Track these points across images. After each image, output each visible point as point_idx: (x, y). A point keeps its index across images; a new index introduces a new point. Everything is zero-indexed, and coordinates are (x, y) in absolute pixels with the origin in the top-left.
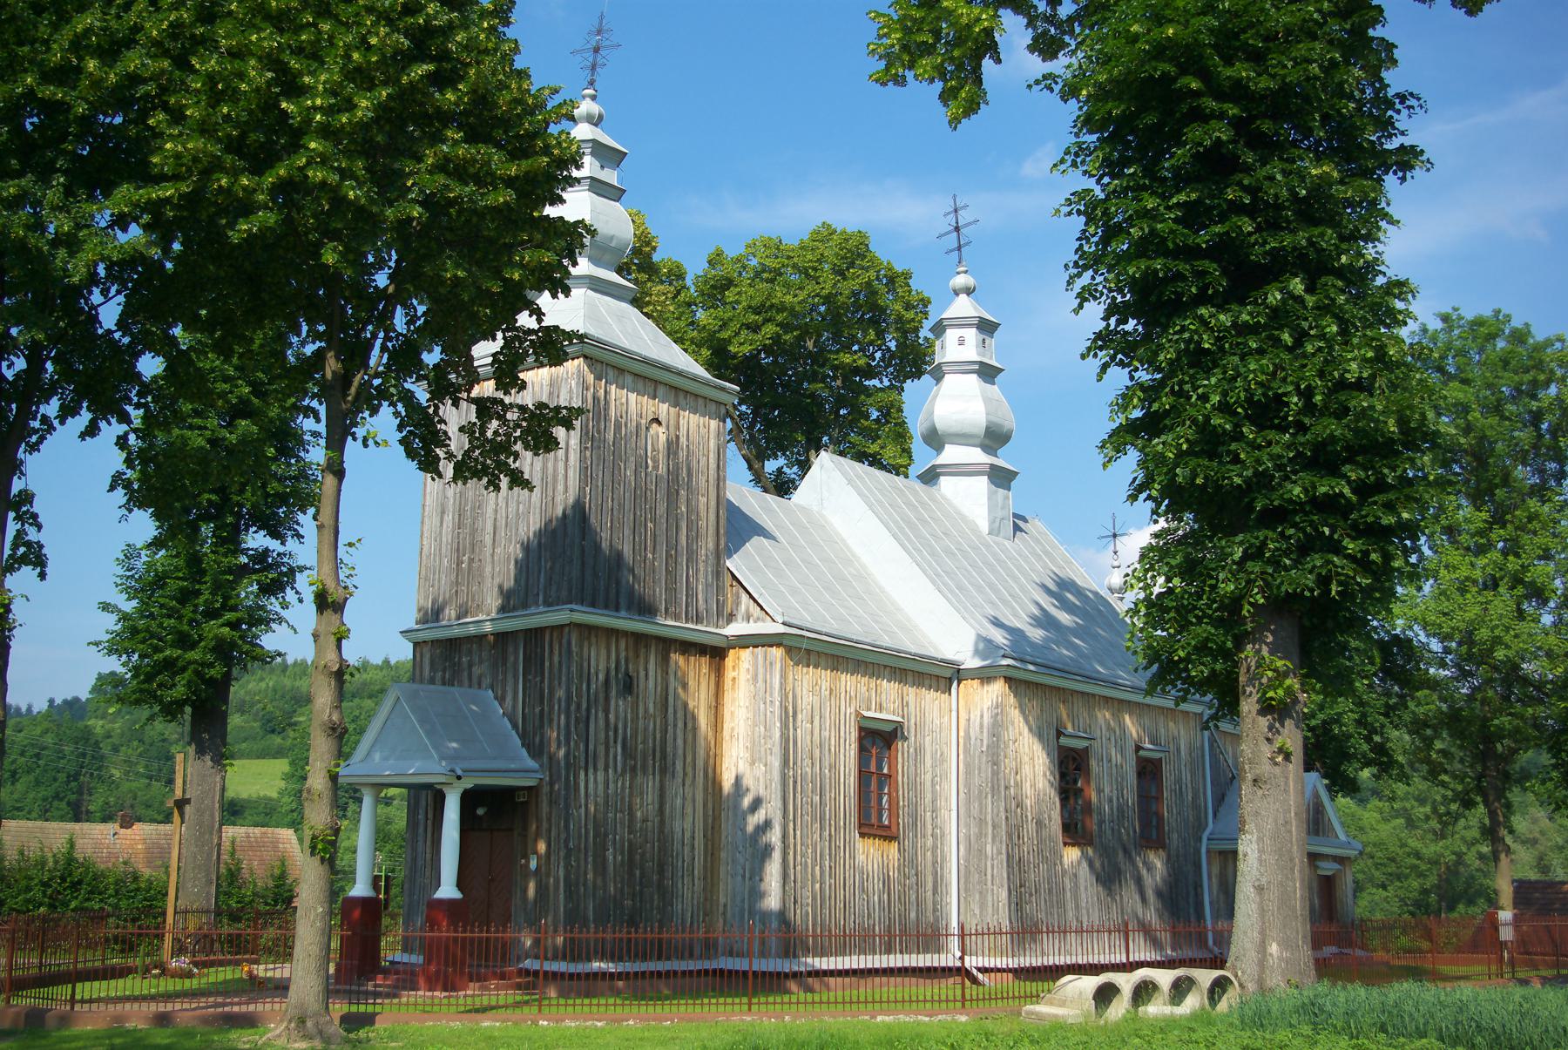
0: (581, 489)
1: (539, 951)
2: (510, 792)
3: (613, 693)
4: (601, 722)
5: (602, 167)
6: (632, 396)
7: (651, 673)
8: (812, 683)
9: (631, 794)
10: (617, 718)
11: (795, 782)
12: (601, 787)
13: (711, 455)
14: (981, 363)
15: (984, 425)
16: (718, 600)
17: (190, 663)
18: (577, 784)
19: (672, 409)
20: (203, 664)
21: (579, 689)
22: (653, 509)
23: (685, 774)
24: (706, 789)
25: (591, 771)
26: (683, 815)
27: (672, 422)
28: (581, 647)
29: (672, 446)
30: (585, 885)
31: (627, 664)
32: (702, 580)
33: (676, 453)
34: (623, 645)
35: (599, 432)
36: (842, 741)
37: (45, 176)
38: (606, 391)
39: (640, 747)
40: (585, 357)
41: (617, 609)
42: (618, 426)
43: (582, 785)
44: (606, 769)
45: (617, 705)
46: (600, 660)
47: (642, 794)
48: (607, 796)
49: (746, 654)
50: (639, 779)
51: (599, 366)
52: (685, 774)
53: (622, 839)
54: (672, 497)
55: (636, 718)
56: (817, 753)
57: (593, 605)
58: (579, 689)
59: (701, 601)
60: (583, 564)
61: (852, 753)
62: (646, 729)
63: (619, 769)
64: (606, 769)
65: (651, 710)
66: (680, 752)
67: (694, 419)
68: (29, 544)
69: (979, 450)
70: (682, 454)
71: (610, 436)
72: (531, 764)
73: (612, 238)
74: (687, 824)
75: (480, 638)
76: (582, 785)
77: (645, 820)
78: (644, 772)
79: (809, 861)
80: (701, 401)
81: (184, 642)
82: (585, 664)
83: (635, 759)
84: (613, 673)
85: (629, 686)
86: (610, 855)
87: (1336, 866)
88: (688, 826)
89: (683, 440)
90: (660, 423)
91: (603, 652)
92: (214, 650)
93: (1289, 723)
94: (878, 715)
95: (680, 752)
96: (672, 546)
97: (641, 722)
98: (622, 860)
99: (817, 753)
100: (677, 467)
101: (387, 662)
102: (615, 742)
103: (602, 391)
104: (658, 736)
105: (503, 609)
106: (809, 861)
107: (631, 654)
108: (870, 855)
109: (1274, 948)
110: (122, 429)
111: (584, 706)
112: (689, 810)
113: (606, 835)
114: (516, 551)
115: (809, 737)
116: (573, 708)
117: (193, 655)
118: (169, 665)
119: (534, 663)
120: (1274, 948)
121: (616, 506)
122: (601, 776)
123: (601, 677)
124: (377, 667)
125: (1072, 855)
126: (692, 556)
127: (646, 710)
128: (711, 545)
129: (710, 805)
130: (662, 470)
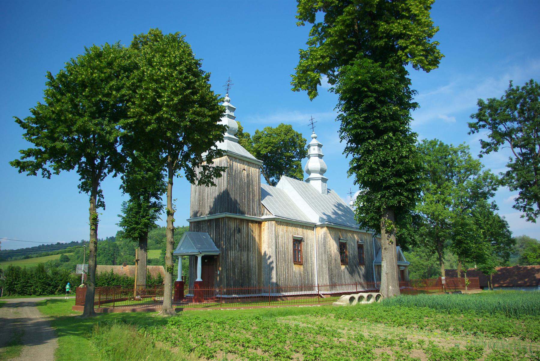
0: (227, 186)
4: (233, 239)
6: (239, 164)
8: (282, 229)
9: (241, 256)
14: (319, 154)
22: (244, 190)
24: (258, 254)
29: (248, 175)
33: (249, 177)
44: (235, 250)
46: (233, 225)
49: (266, 223)
50: (242, 253)
54: (248, 187)
62: (244, 241)
64: (235, 250)
66: (252, 246)
67: (253, 169)
68: (101, 202)
70: (250, 177)
71: (234, 174)
72: (218, 250)
74: (254, 262)
77: (244, 262)
81: (137, 223)
85: (239, 231)
87: (404, 268)
88: (254, 263)
89: (250, 174)
91: (233, 223)
95: (252, 246)
96: (248, 198)
101: (183, 227)
108: (296, 269)
109: (390, 287)
118: (134, 229)
119: (217, 226)
120: (390, 287)
122: (233, 252)
123: (233, 229)
125: (343, 267)
127: (244, 236)
128: (258, 198)
130: (246, 181)
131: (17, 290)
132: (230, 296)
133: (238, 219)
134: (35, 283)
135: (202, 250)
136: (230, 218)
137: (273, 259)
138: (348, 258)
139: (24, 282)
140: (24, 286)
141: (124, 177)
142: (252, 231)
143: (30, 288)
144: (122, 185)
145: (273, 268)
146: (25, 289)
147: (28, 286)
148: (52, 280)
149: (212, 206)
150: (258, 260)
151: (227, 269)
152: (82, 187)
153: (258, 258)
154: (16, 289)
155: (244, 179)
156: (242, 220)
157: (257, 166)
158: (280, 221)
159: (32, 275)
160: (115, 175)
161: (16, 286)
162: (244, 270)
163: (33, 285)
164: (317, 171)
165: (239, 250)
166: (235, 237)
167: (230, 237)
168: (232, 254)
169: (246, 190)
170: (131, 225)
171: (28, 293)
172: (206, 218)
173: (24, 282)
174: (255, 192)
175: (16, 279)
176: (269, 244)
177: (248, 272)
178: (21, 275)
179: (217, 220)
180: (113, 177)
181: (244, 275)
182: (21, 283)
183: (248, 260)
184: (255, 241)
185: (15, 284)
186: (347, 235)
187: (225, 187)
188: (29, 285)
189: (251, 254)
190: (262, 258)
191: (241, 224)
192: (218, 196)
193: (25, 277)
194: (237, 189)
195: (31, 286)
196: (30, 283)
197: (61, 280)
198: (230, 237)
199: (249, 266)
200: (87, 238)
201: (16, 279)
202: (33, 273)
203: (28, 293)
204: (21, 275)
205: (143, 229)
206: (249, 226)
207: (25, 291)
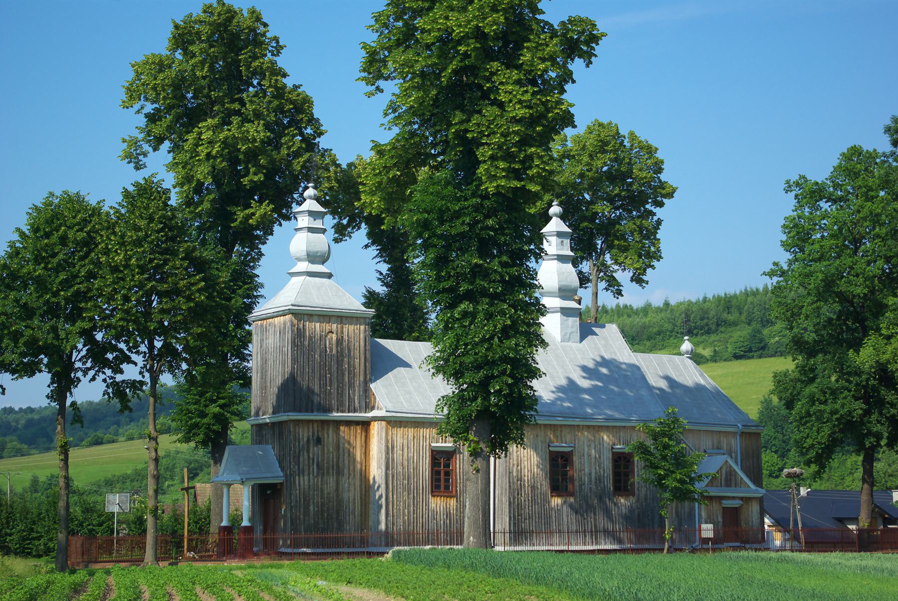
0: (293, 368)
1: (284, 545)
2: (275, 485)
3: (312, 445)
4: (306, 457)
5: (315, 220)
6: (318, 325)
7: (330, 435)
8: (400, 436)
9: (322, 484)
10: (314, 455)
11: (393, 476)
12: (306, 482)
13: (361, 341)
14: (557, 255)
15: (557, 287)
16: (366, 402)
17: (204, 424)
18: (295, 482)
19: (339, 326)
20: (209, 425)
21: (294, 445)
22: (330, 369)
23: (350, 474)
24: (361, 480)
25: (301, 476)
26: (349, 491)
27: (339, 331)
28: (295, 428)
29: (340, 341)
30: (299, 519)
31: (318, 432)
32: (357, 394)
33: (342, 344)
34: (316, 425)
35: (301, 342)
36: (421, 457)
37: (58, 317)
38: (304, 325)
39: (326, 465)
40: (292, 314)
41: (312, 412)
42: (310, 338)
43: (297, 482)
44: (309, 475)
45: (314, 450)
46: (304, 434)
47: (327, 484)
48: (309, 485)
49: (376, 423)
50: (325, 478)
51: (300, 316)
52: (350, 474)
53: (318, 502)
54: (339, 363)
55: (323, 454)
56: (406, 463)
57: (300, 412)
58: (294, 445)
59: (356, 401)
60: (294, 397)
61: (427, 462)
62: (328, 458)
63: (315, 474)
64: (309, 475)
65: (331, 449)
66: (347, 465)
67: (351, 327)
68: (78, 416)
69: (558, 299)
70: (345, 344)
71: (306, 343)
72: (281, 474)
73: (318, 252)
74: (351, 494)
75: (267, 424)
76: (297, 482)
77: (329, 494)
78: (328, 473)
79: (401, 508)
80: (354, 319)
81: (203, 415)
82: (297, 435)
83: (323, 470)
84: (311, 437)
85: (319, 441)
86: (311, 508)
87: (741, 502)
88: (351, 495)
89: (346, 338)
90: (333, 333)
91: (306, 429)
92: (213, 418)
93: (479, 459)
94: (443, 445)
95: (347, 465)
96: (340, 381)
97: (326, 455)
98: (318, 510)
99: (406, 463)
100: (342, 349)
101: (667, 304)
102: (313, 464)
103: (302, 326)
104: (335, 460)
105: (274, 413)
106: (401, 508)
107: (320, 429)
108: (437, 504)
109: (471, 538)
110: (103, 376)
111: (297, 451)
112: (352, 488)
113: (309, 500)
114: (276, 390)
115: (401, 457)
116: (292, 452)
117: (205, 421)
118: (196, 425)
119: (281, 434)
120: (471, 538)
121: (311, 371)
122: (306, 478)
123: (305, 439)
124: (659, 310)
125: (556, 501)
126: (351, 385)
127: (328, 450)
128: (362, 379)
129: (363, 486)
130: (334, 352)
131: (12, 546)
132: (295, 551)
133: (317, 421)
134: (48, 532)
135: (248, 476)
136: (297, 422)
137: (382, 491)
138: (577, 484)
139: (24, 531)
140: (24, 539)
141: (108, 379)
142: (349, 443)
143: (37, 543)
144: (106, 391)
145: (381, 506)
146: (28, 544)
147: (34, 539)
148: (81, 525)
149: (275, 403)
150: (361, 490)
151: (292, 508)
152: (52, 397)
153: (361, 486)
154: (10, 545)
155: (331, 349)
156: (324, 423)
157: (362, 320)
158: (394, 422)
159: (40, 514)
160: (93, 379)
161: (8, 538)
162: (328, 508)
163: (42, 536)
164: (555, 293)
165: (318, 475)
166: (308, 452)
167: (299, 452)
168: (303, 482)
169: (334, 368)
170: (191, 418)
171: (34, 553)
172: (268, 421)
173: (24, 531)
174: (354, 368)
175: (8, 523)
176: (379, 461)
177: (338, 513)
178: (18, 515)
179: (281, 423)
180: (90, 381)
181: (328, 515)
182: (19, 532)
183: (337, 489)
184: (354, 459)
185: (7, 534)
186: (600, 435)
187: (288, 369)
188: (35, 535)
189: (345, 482)
190: (366, 487)
191: (323, 429)
192: (282, 384)
193: (27, 519)
194: (313, 371)
195: (38, 538)
196: (37, 532)
197: (100, 525)
198: (299, 452)
199: (340, 502)
200: (56, 471)
201: (8, 523)
202: (44, 509)
203: (34, 553)
204: (18, 515)
205: (213, 425)
206: (341, 433)
207: (28, 548)
